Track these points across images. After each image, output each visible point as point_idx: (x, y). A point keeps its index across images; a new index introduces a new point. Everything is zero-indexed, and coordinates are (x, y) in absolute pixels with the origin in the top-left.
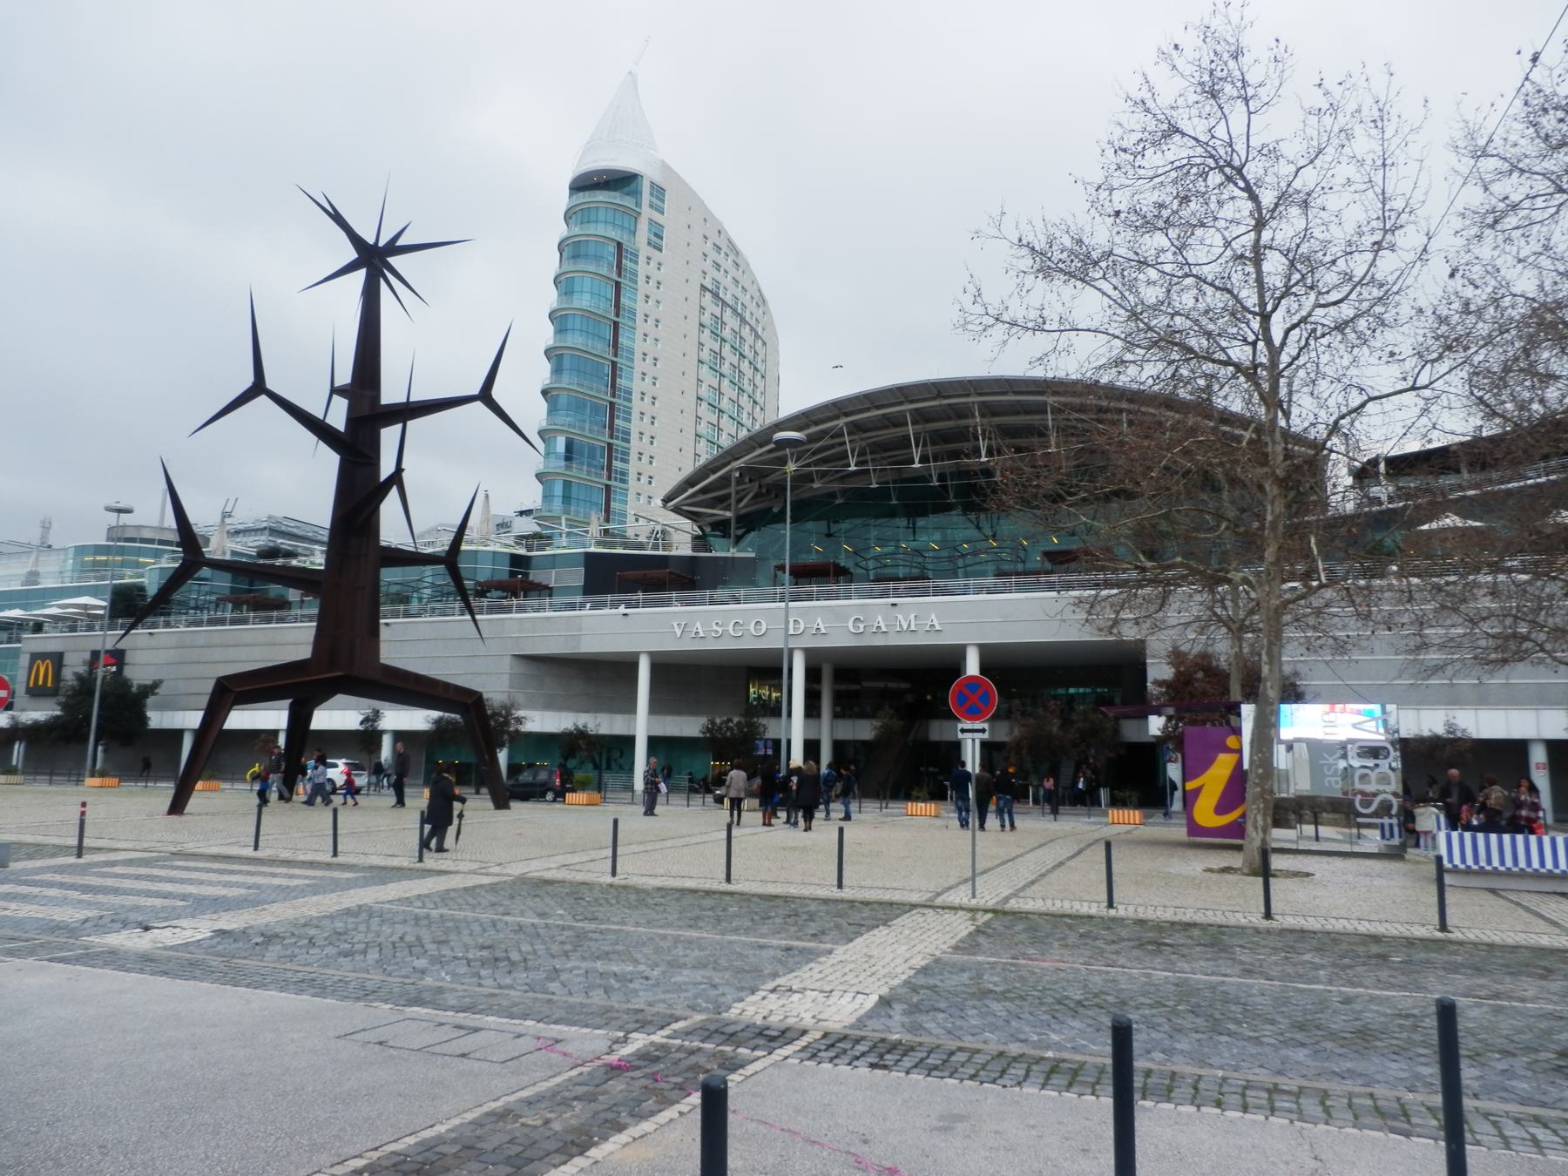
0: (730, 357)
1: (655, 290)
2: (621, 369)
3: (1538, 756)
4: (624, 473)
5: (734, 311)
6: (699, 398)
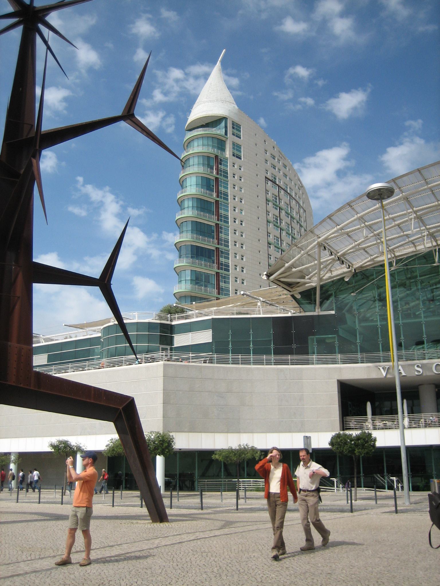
0: (286, 220)
1: (239, 203)
2: (221, 228)
3: (362, 485)
4: (227, 217)
5: (286, 191)
6: (269, 244)
